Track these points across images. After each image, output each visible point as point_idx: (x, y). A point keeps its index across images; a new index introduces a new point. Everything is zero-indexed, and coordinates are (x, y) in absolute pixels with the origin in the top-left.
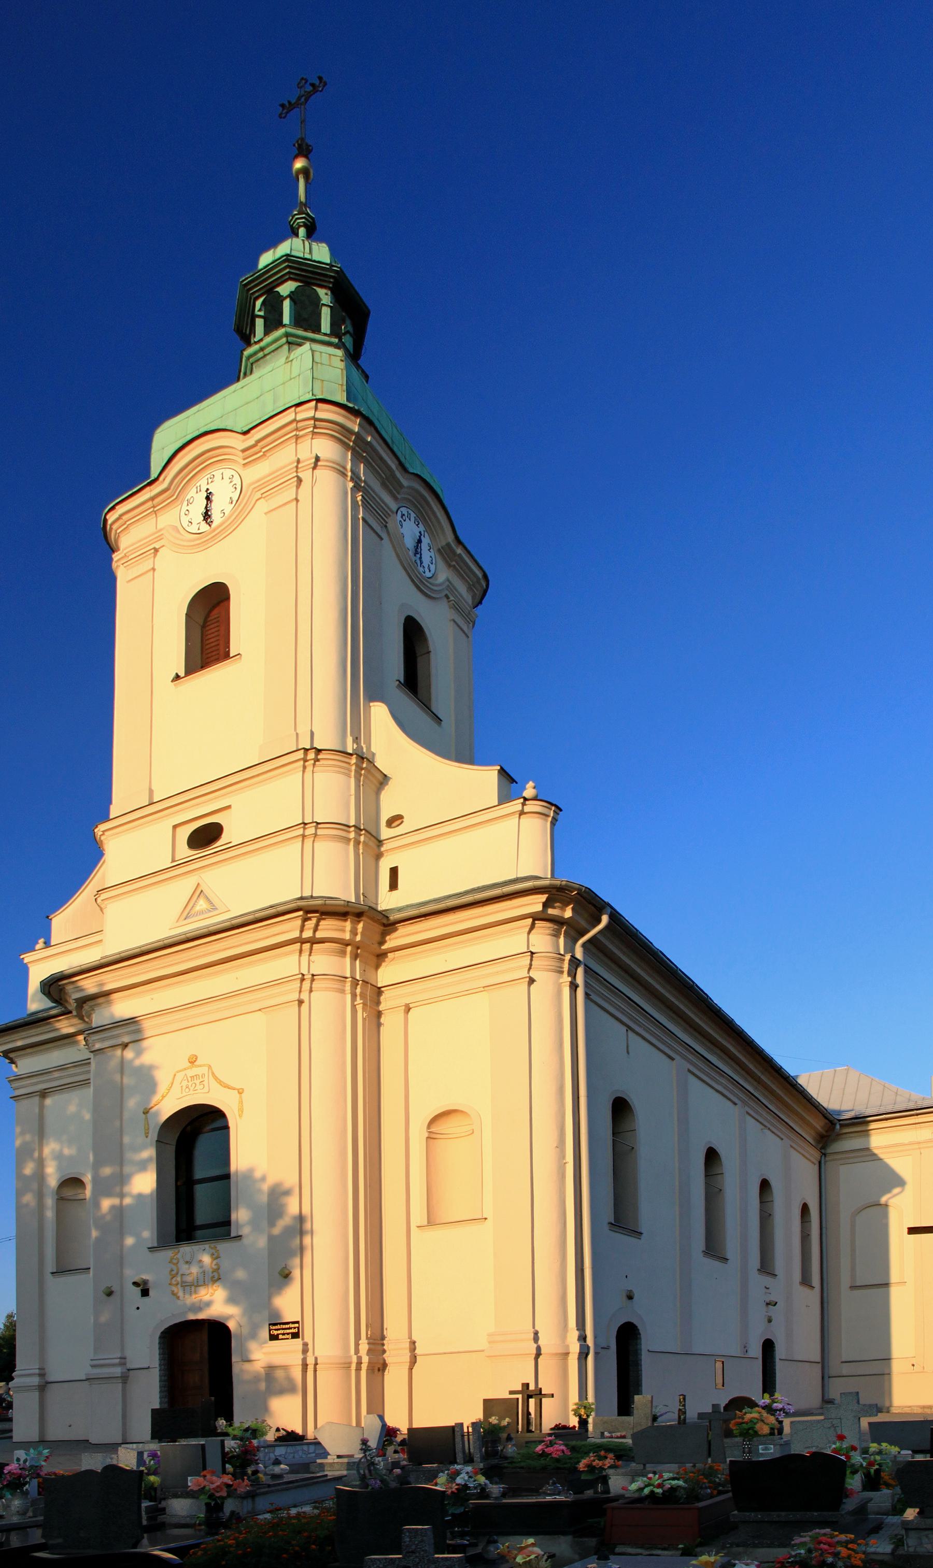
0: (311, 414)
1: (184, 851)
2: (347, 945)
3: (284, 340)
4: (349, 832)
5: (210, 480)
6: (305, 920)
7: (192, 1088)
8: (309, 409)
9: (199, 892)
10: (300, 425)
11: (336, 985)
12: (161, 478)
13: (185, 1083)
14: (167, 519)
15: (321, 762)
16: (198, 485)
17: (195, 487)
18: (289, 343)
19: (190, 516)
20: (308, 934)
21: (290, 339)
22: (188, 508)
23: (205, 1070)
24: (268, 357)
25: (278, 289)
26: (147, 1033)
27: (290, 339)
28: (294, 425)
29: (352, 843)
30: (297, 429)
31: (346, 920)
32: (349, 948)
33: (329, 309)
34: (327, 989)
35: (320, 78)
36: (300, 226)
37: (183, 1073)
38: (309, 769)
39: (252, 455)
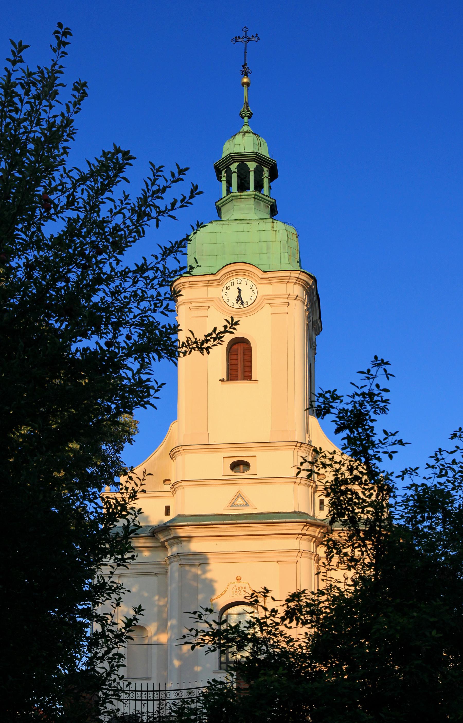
0: (297, 276)
1: (229, 471)
2: (314, 538)
3: (253, 196)
4: (311, 482)
5: (239, 282)
6: (305, 526)
7: (239, 593)
8: (297, 273)
9: (239, 495)
10: (291, 278)
11: (309, 556)
12: (217, 274)
13: (235, 590)
14: (214, 292)
15: (302, 448)
16: (233, 281)
17: (230, 282)
18: (255, 198)
19: (228, 296)
20: (303, 532)
21: (256, 197)
22: (226, 291)
23: (246, 585)
24: (242, 200)
25: (247, 163)
26: (210, 561)
27: (256, 197)
28: (289, 277)
29: (310, 487)
30: (289, 279)
31: (318, 528)
32: (314, 539)
33: (268, 179)
34: (307, 557)
35: (257, 35)
36: (246, 116)
37: (234, 585)
38: (296, 450)
39: (263, 281)
